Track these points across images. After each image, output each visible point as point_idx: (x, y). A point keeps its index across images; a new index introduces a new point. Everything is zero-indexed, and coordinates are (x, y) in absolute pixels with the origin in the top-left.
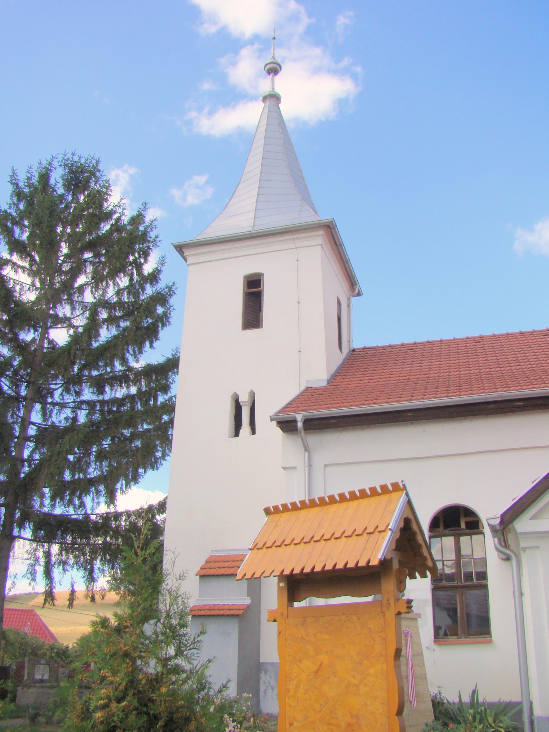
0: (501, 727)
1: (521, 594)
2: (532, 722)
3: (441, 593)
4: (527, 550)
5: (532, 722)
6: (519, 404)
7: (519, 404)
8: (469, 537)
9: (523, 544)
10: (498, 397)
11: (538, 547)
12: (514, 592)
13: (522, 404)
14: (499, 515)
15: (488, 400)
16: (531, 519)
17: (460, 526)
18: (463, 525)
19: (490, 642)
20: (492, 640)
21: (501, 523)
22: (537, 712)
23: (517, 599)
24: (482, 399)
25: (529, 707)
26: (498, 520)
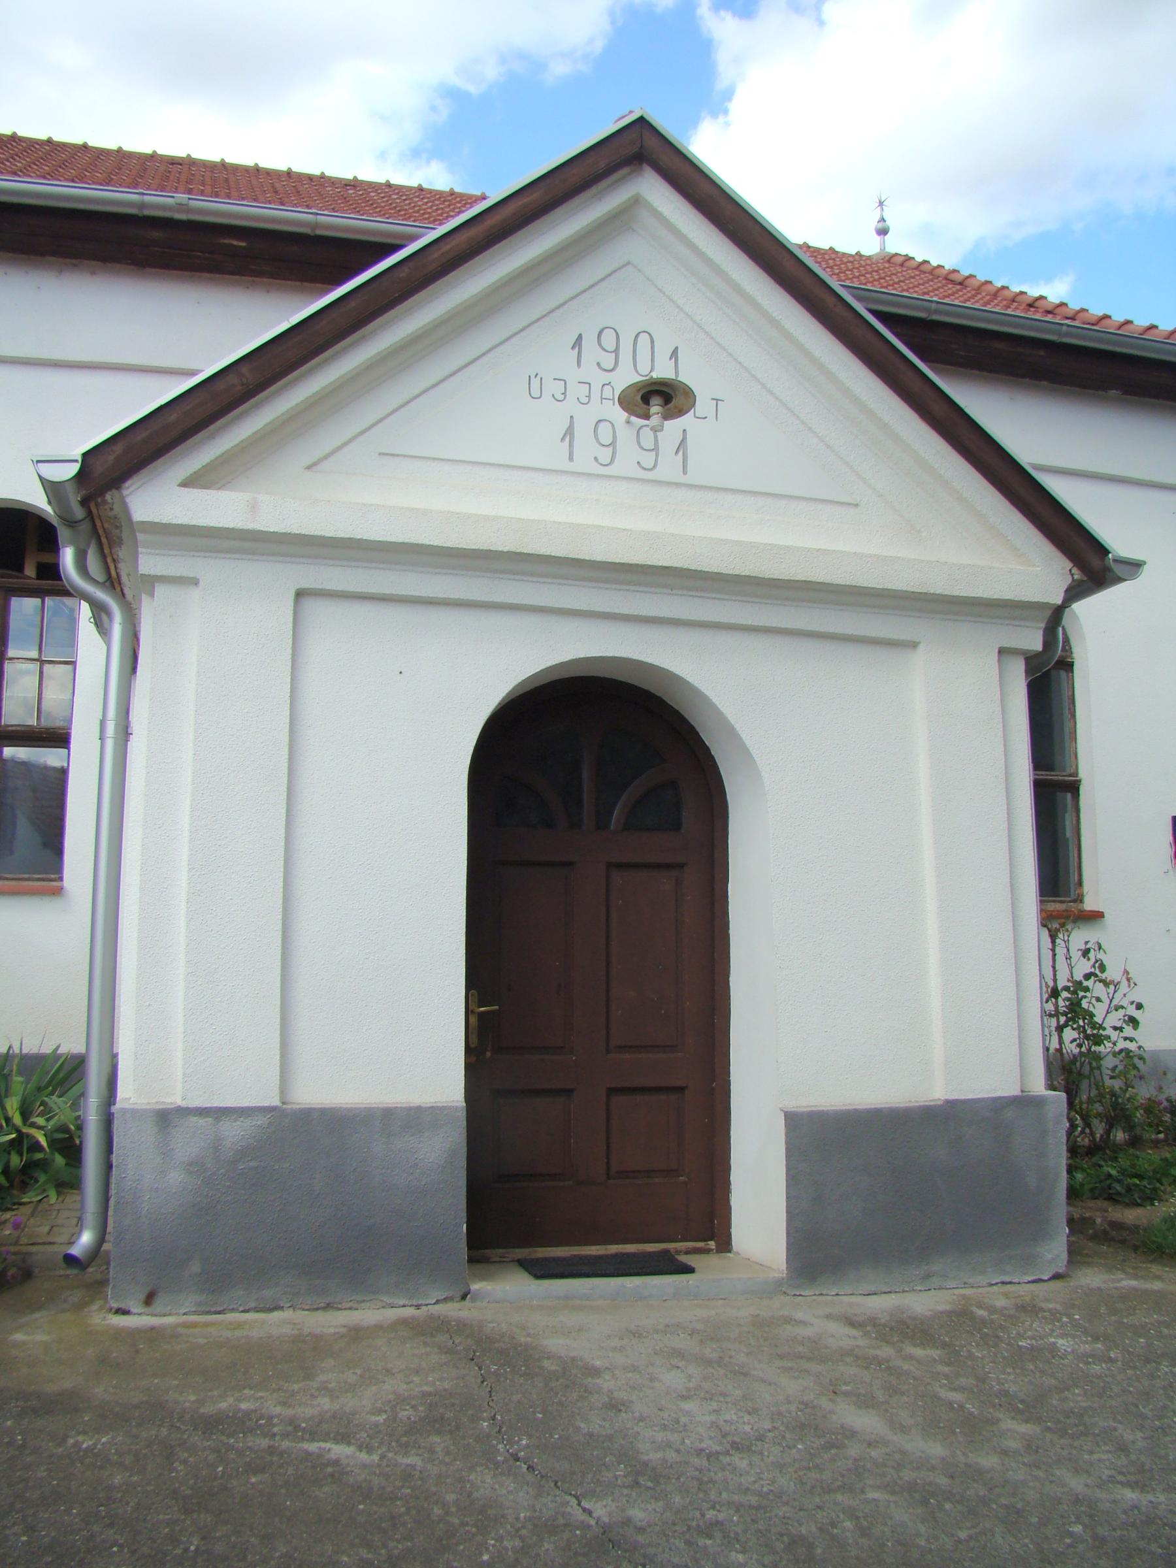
0: (40, 1128)
1: (125, 732)
2: (108, 1122)
3: (627, 1056)
4: (160, 590)
5: (108, 1122)
6: (235, 243)
7: (235, 243)
8: (38, 601)
9: (149, 563)
10: (181, 207)
11: (195, 582)
12: (103, 723)
13: (243, 244)
14: (78, 452)
15: (147, 212)
16: (185, 484)
17: (20, 568)
18: (30, 571)
19: (58, 892)
20: (62, 888)
21: (81, 476)
22: (127, 1093)
23: (110, 744)
24: (130, 204)
25: (104, 1079)
26: (73, 469)
